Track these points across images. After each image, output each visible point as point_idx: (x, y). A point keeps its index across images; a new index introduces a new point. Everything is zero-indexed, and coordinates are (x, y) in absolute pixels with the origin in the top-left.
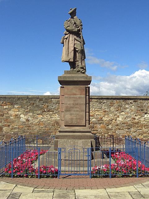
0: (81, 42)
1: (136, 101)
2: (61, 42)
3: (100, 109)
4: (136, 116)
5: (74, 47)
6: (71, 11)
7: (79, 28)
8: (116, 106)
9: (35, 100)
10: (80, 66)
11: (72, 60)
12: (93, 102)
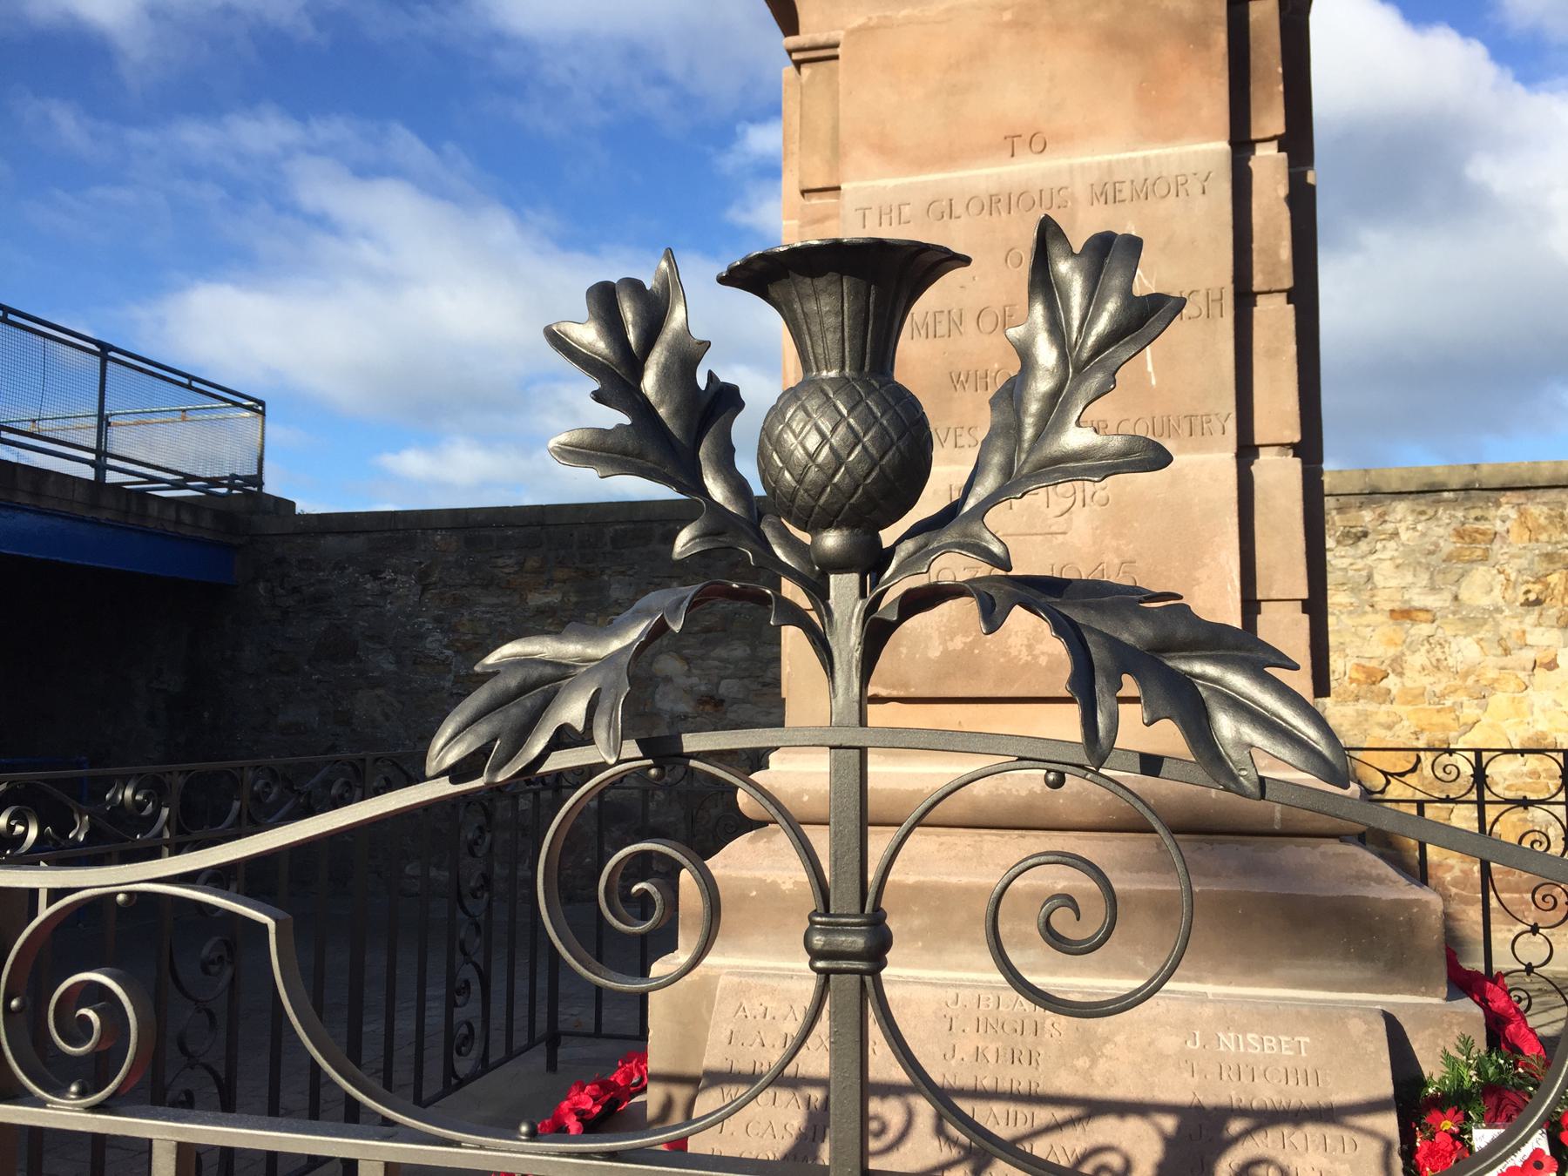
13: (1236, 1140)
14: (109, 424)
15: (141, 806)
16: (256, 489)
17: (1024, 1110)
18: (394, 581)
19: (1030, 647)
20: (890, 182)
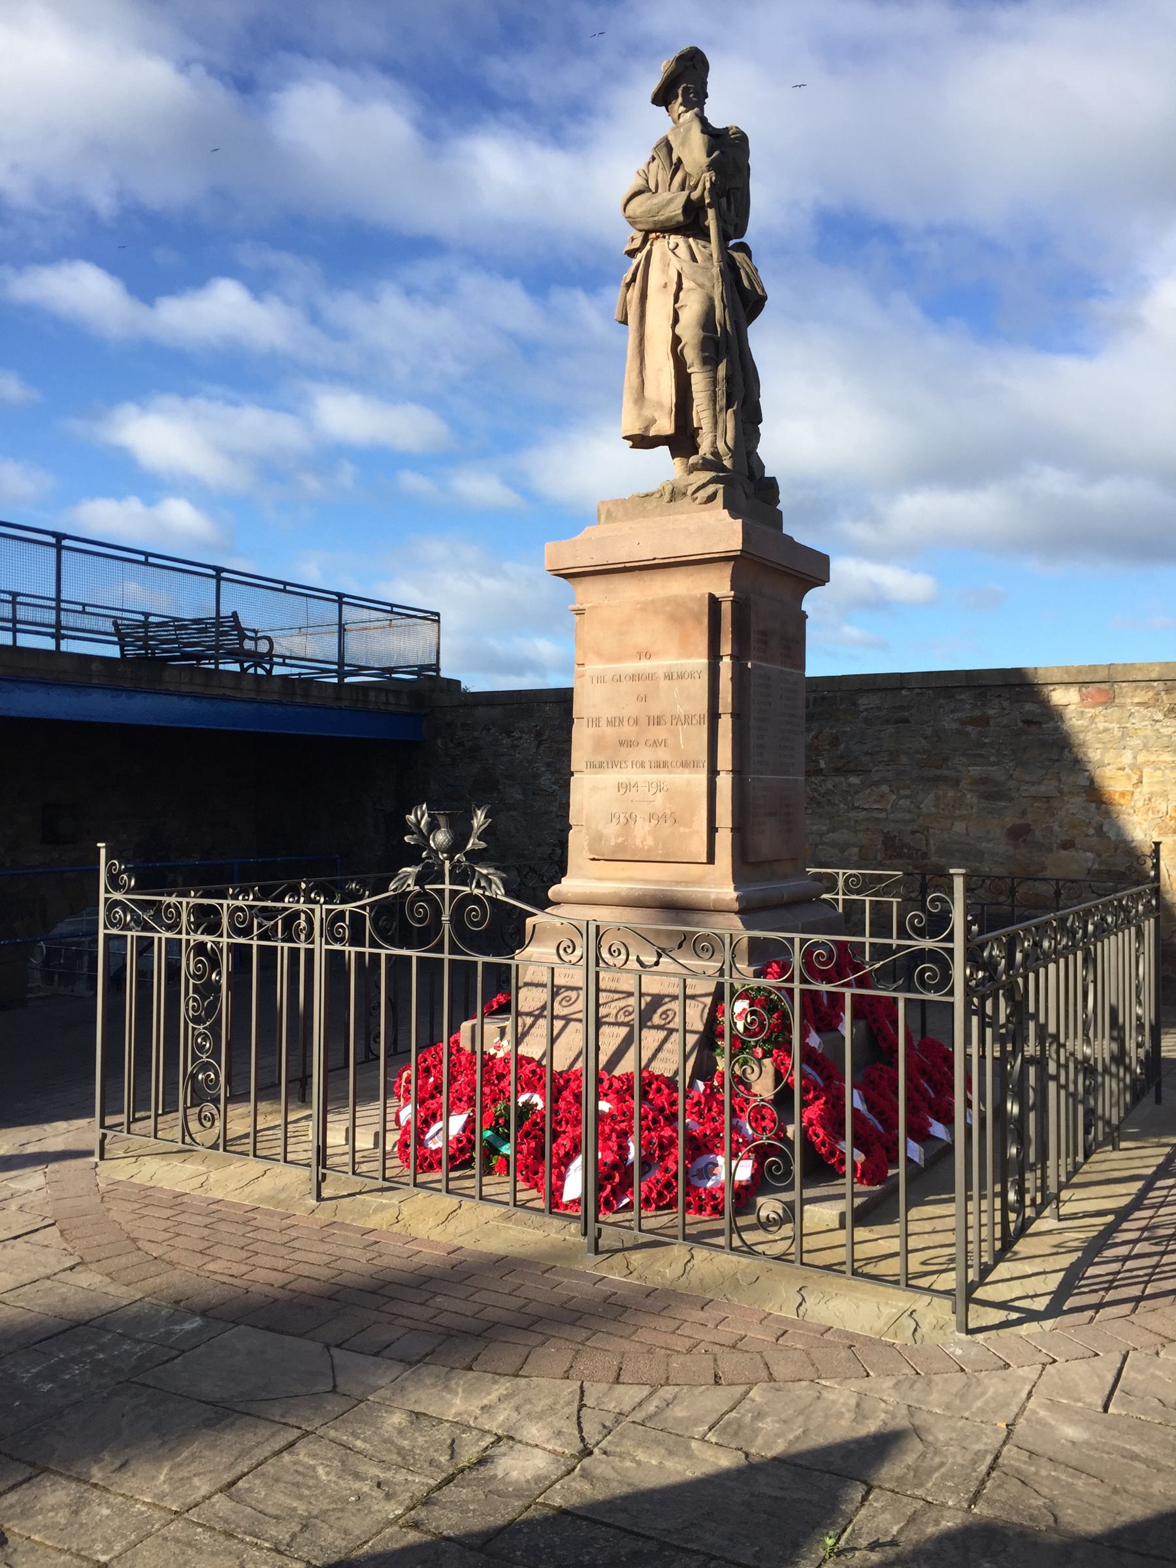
13: (666, 1003)
14: (345, 630)
15: (358, 891)
16: (435, 674)
17: (611, 995)
18: (520, 738)
19: (642, 842)
20: (601, 667)
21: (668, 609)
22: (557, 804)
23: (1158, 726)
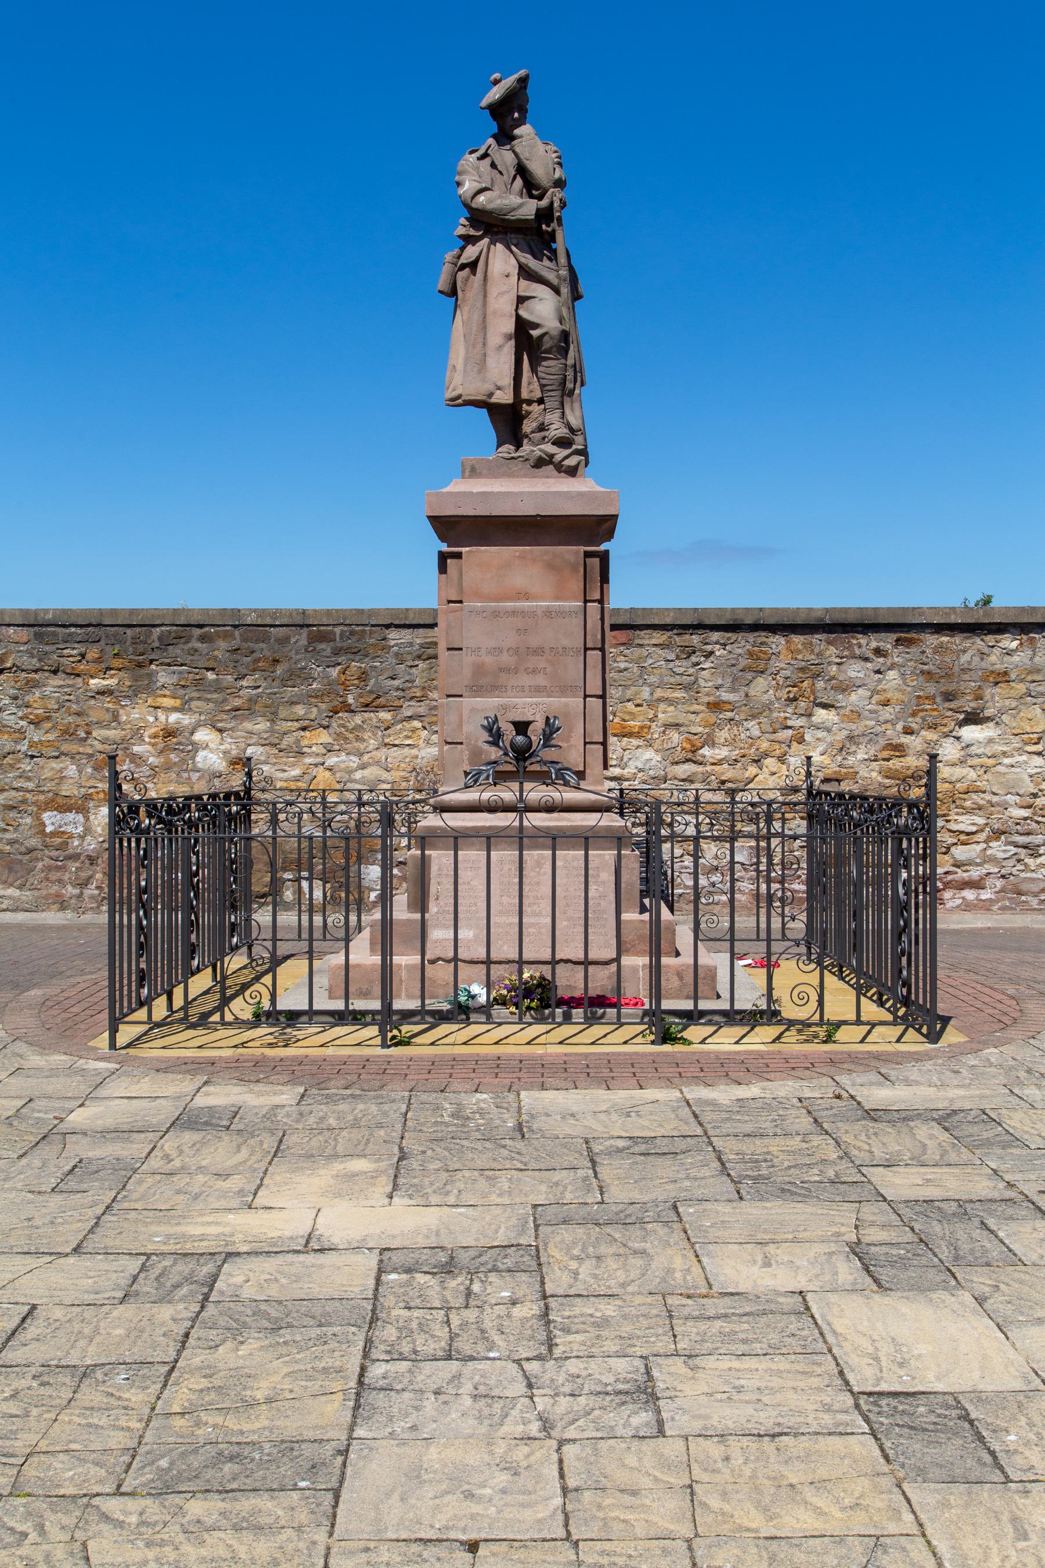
0: (557, 291)
1: (910, 642)
2: (443, 283)
3: (687, 687)
4: (908, 731)
5: (518, 318)
6: (495, 94)
7: (544, 203)
8: (788, 673)
9: (284, 641)
10: (557, 430)
11: (505, 397)
12: (641, 646)
21: (546, 558)
22: (26, 741)
23: (671, 665)
